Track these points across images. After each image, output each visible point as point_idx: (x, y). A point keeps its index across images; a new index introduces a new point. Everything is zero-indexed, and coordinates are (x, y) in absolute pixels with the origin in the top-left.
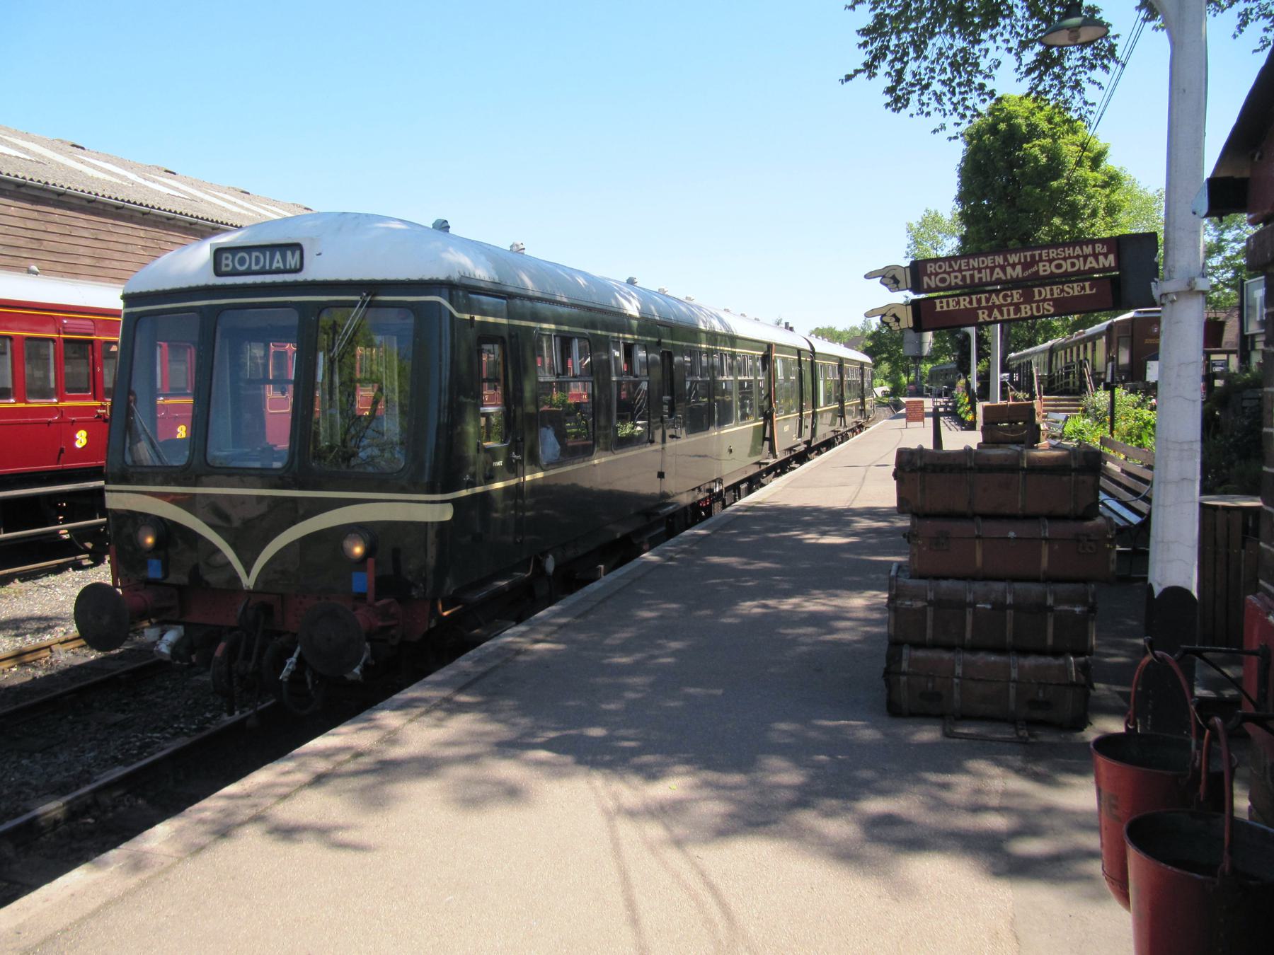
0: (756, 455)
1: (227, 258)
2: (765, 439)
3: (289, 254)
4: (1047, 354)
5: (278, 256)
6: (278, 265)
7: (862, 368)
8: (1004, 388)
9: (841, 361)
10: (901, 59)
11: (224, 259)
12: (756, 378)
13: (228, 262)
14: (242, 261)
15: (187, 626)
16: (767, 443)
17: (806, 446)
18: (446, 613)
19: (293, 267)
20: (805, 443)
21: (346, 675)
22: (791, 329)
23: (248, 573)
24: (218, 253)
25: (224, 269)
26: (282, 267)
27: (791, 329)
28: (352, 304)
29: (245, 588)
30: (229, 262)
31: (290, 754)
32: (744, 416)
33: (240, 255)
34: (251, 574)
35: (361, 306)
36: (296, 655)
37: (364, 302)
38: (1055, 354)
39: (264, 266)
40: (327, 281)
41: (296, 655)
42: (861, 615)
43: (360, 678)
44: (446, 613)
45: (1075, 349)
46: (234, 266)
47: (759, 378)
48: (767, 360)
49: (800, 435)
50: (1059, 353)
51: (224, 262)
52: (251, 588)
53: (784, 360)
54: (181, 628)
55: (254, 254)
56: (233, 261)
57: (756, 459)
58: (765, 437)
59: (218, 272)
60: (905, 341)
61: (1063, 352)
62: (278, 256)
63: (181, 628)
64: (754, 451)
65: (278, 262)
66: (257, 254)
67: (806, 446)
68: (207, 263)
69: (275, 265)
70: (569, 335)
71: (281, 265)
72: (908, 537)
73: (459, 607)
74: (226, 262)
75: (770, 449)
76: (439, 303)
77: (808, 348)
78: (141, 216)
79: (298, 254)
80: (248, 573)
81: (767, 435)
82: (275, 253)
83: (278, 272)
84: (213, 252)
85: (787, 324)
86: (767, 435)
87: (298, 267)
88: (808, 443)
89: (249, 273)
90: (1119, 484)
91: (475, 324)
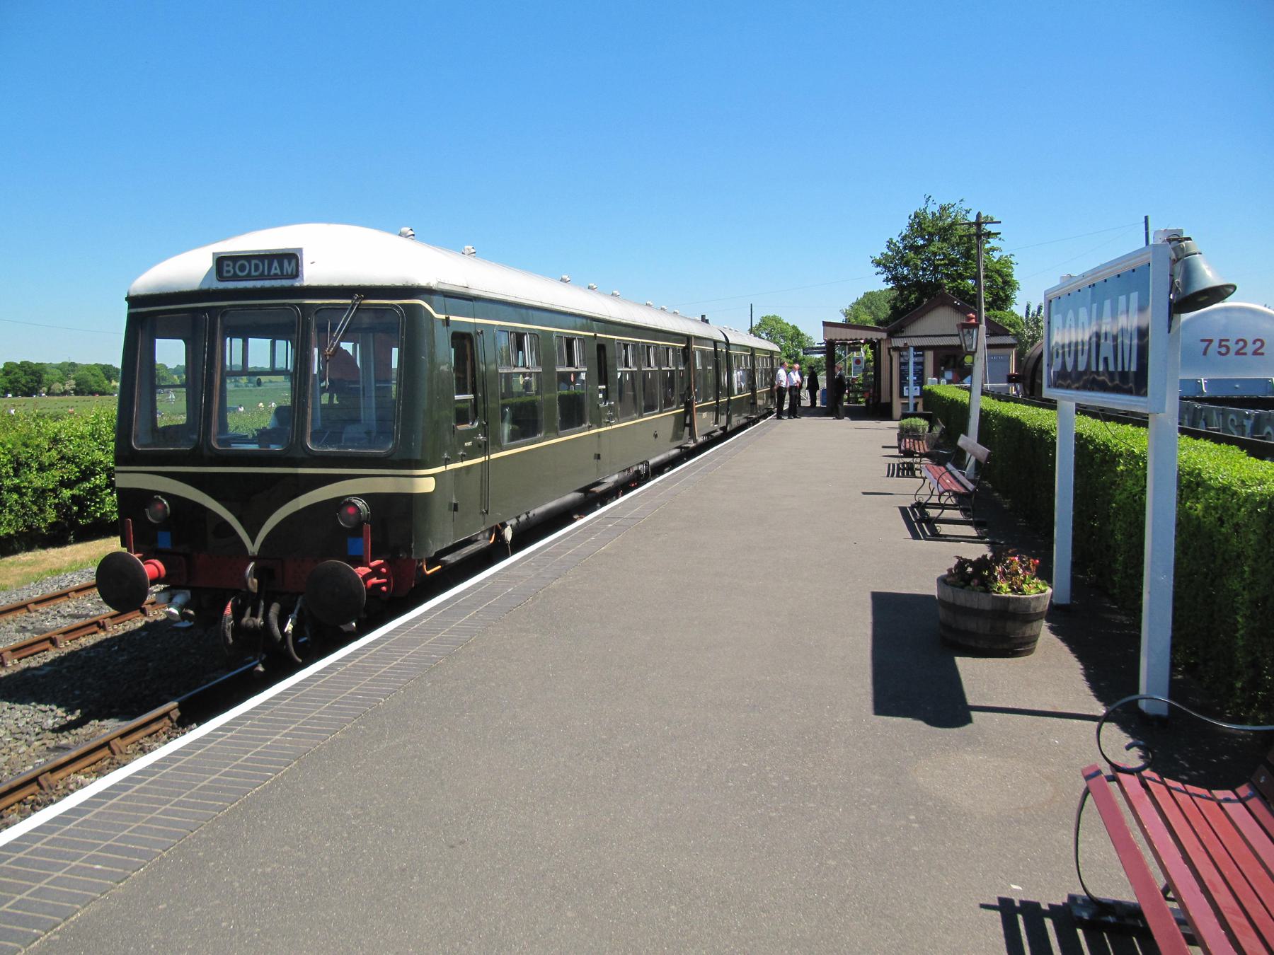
0: (678, 440)
1: (228, 265)
2: (686, 425)
3: (286, 263)
5: (276, 264)
6: (276, 272)
7: (772, 358)
8: (903, 367)
9: (753, 350)
11: (225, 265)
12: (677, 368)
13: (229, 268)
14: (242, 268)
15: (193, 590)
16: (687, 429)
17: (722, 432)
19: (290, 273)
20: (721, 429)
21: (342, 627)
22: (707, 321)
23: (253, 540)
24: (221, 261)
25: (225, 274)
26: (279, 273)
27: (707, 321)
28: (343, 308)
29: (250, 554)
30: (230, 268)
32: (668, 404)
33: (239, 263)
34: (256, 543)
36: (296, 611)
37: (354, 305)
39: (263, 271)
41: (296, 611)
43: (355, 630)
44: (429, 572)
46: (235, 272)
48: (686, 355)
49: (716, 422)
51: (225, 268)
52: (256, 554)
53: (702, 352)
54: (188, 592)
55: (253, 262)
56: (234, 268)
57: (678, 443)
58: (684, 423)
60: (951, 600)
62: (276, 264)
63: (188, 592)
64: (676, 436)
65: (276, 269)
66: (257, 262)
67: (722, 432)
68: (212, 267)
69: (273, 272)
70: (522, 331)
71: (278, 272)
73: (439, 567)
74: (228, 269)
75: (690, 435)
76: (420, 305)
77: (724, 340)
80: (253, 540)
81: (688, 421)
82: (273, 262)
83: (276, 277)
84: (215, 259)
85: (703, 317)
86: (688, 421)
87: (294, 273)
88: (724, 428)
89: (249, 277)
90: (473, 375)
91: (450, 323)
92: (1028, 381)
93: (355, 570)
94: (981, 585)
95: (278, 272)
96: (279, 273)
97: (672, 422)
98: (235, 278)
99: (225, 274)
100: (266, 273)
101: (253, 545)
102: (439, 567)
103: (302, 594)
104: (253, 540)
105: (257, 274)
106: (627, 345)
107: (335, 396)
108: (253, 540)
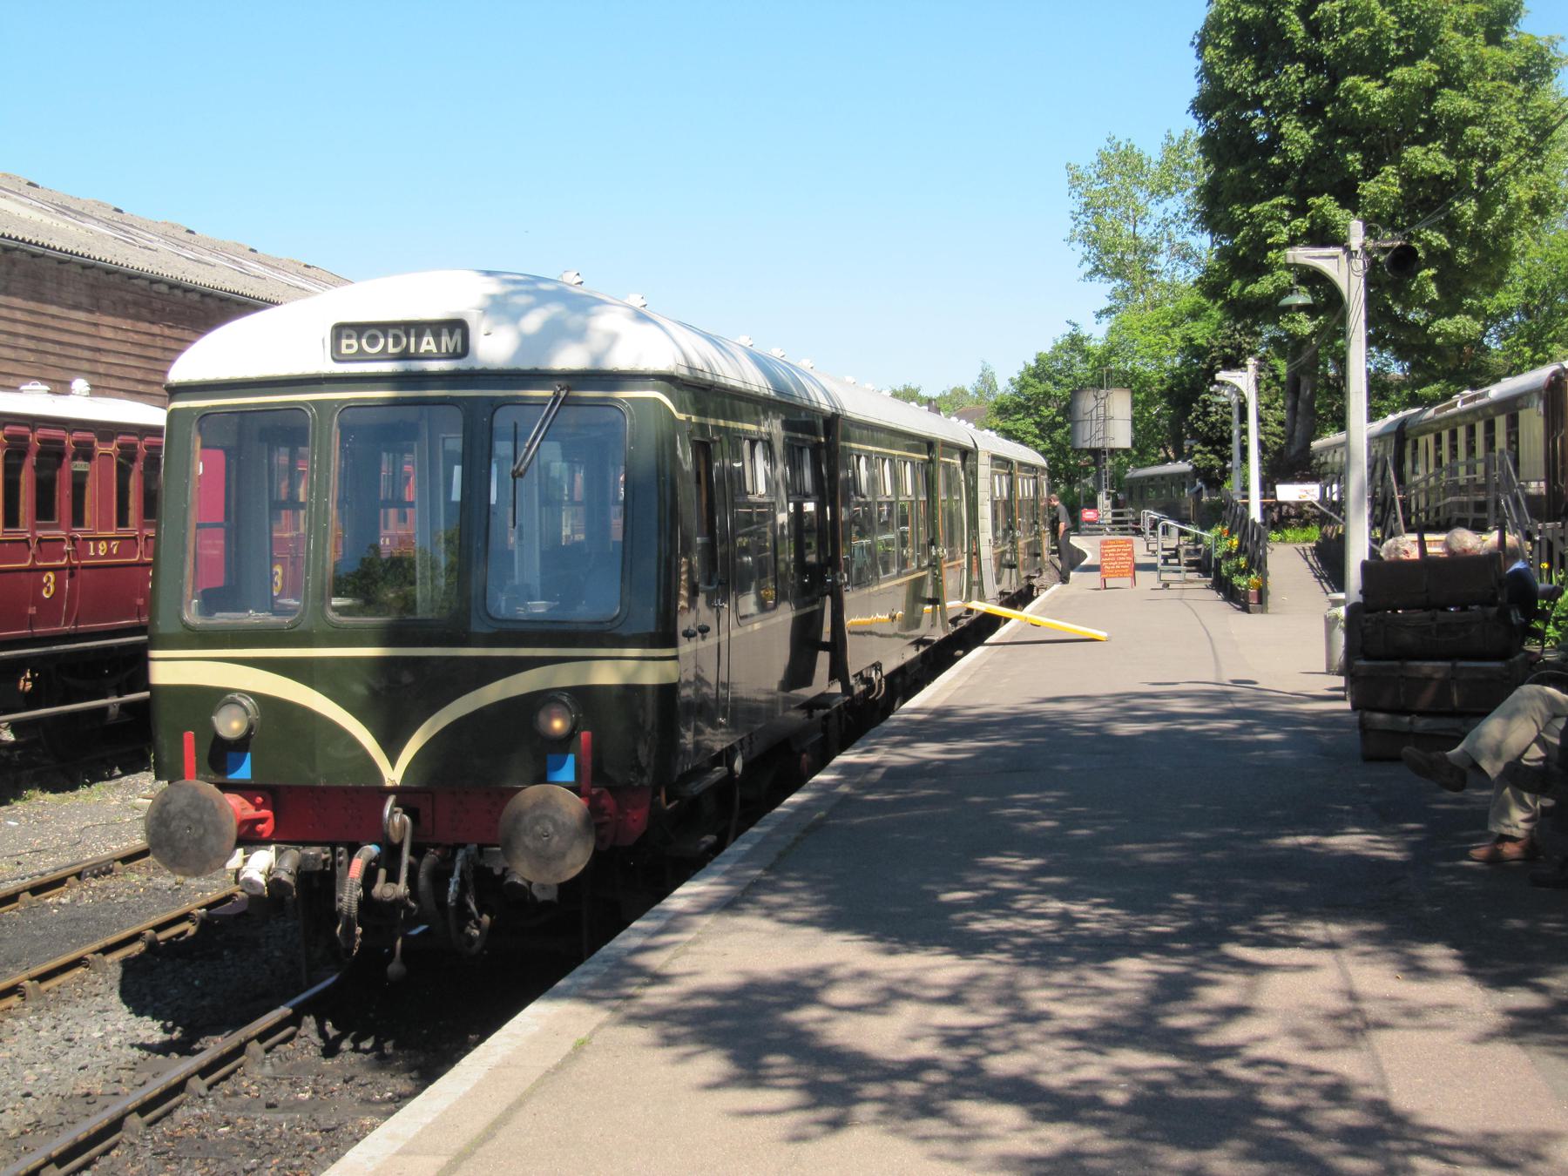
4: (1392, 442)
6: (428, 348)
10: (1334, 417)
12: (917, 499)
18: (669, 807)
19: (451, 350)
31: (766, 817)
35: (554, 404)
37: (556, 398)
38: (1409, 444)
40: (519, 370)
42: (1137, 976)
44: (669, 807)
45: (1462, 432)
47: (920, 499)
50: (1422, 441)
55: (391, 332)
59: (338, 357)
61: (1431, 438)
72: (1323, 520)
73: (676, 802)
78: (80, 271)
79: (458, 337)
87: (459, 350)
92: (198, 305)
93: (293, 884)
94: (1469, 308)
95: (433, 347)
96: (435, 351)
97: (903, 591)
98: (361, 357)
99: (344, 351)
100: (412, 350)
101: (393, 768)
102: (676, 802)
103: (464, 846)
104: (393, 762)
105: (396, 350)
106: (801, 449)
107: (1423, 519)
108: (393, 762)
